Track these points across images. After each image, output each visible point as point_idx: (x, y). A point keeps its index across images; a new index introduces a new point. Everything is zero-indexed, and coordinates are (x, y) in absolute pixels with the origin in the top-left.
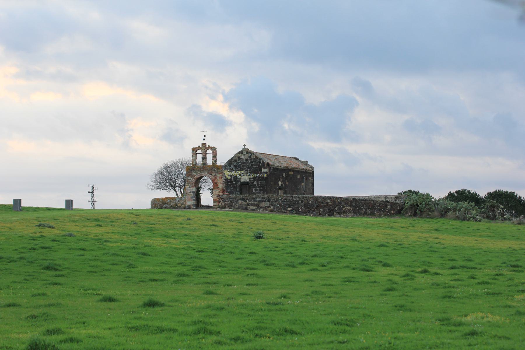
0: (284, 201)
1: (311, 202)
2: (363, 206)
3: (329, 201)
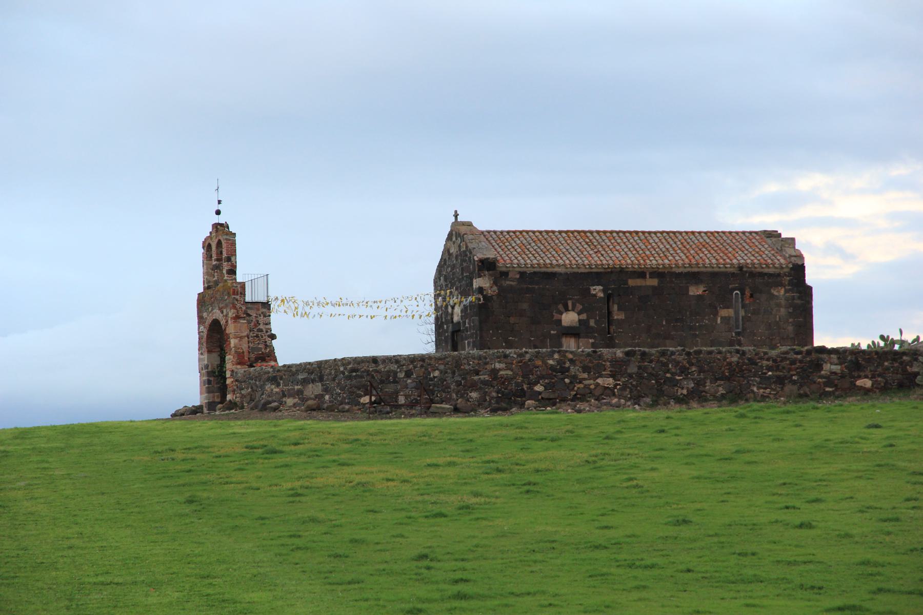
0: (349, 378)
1: (437, 373)
2: (684, 371)
3: (498, 366)
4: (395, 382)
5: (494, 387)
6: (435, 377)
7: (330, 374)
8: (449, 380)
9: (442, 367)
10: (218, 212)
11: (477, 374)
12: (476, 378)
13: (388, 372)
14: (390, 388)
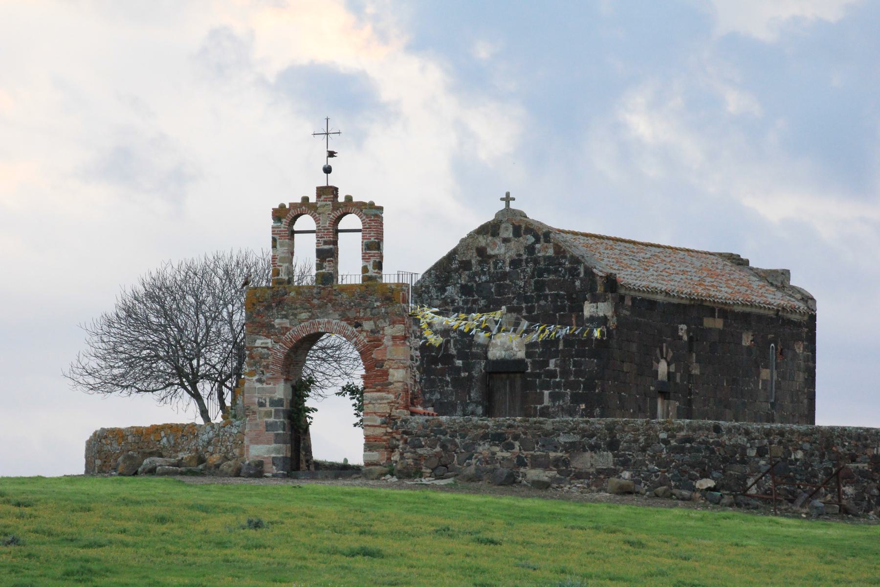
1: (800, 455)
5: (874, 481)
6: (797, 460)
7: (636, 441)
9: (807, 446)
10: (328, 170)
12: (852, 466)
13: (734, 446)
14: (736, 470)
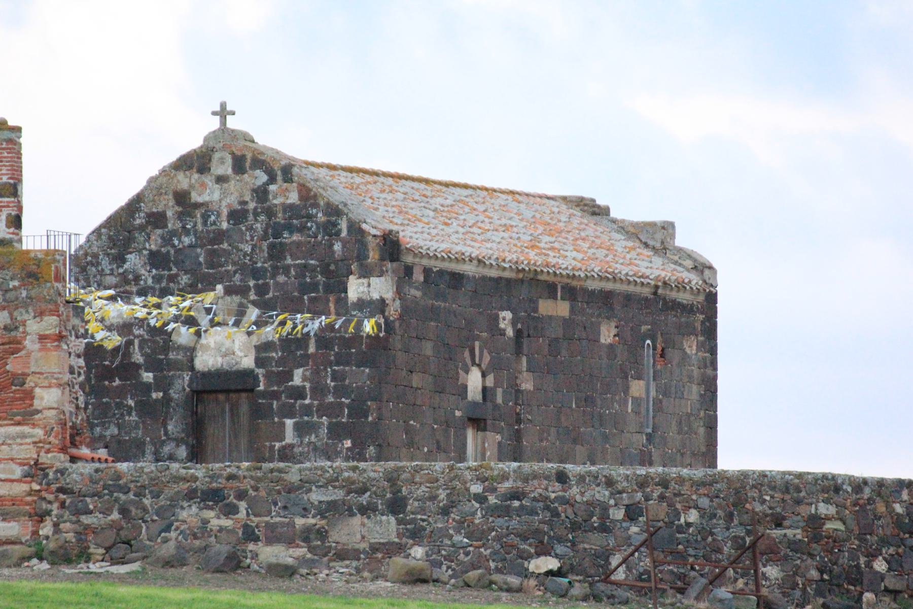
0: (503, 511)
3: (824, 509)
4: (605, 528)
6: (689, 525)
7: (433, 498)
8: (720, 534)
9: (704, 502)
11: (779, 525)
12: (776, 533)
13: (589, 503)
14: (593, 542)
